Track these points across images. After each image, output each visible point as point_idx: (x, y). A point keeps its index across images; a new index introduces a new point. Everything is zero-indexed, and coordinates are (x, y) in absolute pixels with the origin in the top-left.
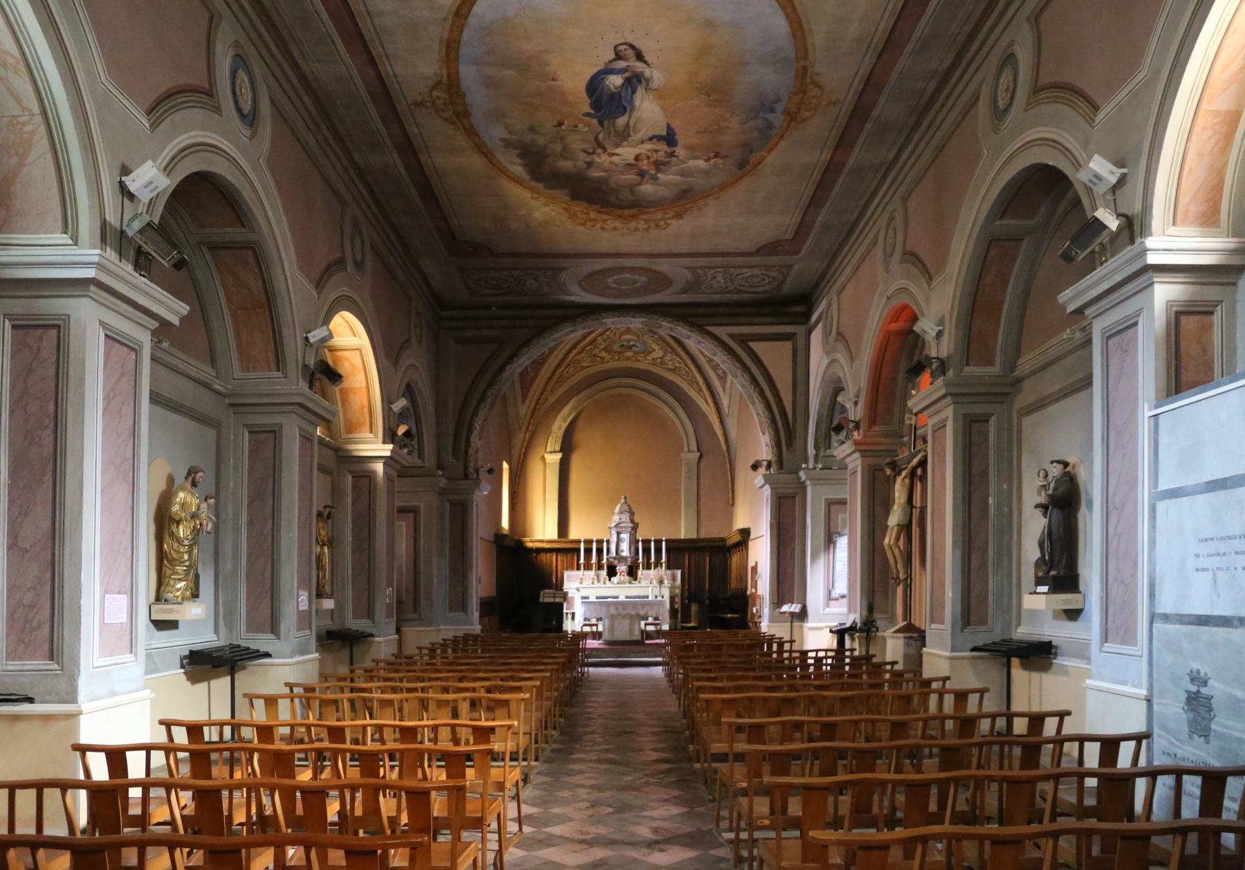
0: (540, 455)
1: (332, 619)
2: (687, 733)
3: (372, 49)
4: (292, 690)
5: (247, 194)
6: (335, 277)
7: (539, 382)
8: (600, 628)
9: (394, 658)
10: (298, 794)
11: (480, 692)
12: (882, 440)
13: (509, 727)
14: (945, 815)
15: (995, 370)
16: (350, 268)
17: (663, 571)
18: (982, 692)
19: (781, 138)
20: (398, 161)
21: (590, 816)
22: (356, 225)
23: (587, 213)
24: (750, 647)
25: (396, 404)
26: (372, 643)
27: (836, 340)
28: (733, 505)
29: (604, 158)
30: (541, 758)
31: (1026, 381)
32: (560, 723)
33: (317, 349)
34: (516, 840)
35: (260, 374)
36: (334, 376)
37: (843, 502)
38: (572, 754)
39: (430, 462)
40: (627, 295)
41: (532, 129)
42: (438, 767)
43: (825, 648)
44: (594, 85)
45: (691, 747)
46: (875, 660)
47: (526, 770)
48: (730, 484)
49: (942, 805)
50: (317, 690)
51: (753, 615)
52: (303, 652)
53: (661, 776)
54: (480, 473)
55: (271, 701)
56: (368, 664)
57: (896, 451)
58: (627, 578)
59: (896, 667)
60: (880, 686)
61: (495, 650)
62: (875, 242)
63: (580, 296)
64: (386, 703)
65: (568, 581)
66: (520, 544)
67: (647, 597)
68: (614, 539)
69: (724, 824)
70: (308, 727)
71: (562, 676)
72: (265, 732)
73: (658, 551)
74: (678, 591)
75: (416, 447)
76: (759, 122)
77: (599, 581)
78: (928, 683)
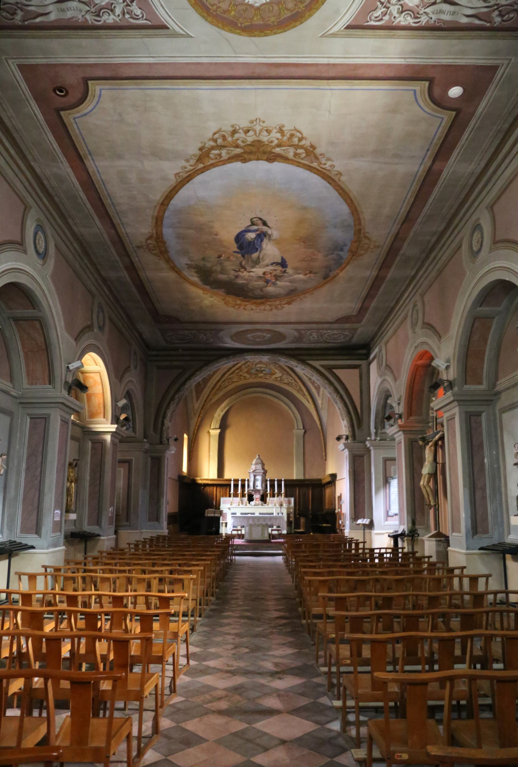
0: (207, 431)
1: (75, 525)
2: (298, 600)
3: (114, 221)
4: (46, 570)
5: (38, 293)
6: (87, 334)
7: (206, 391)
8: (243, 532)
9: (112, 550)
10: (44, 640)
11: (165, 574)
12: (416, 425)
13: (182, 597)
14: (466, 658)
15: (483, 387)
16: (96, 330)
17: (282, 498)
18: (487, 577)
19: (348, 264)
20: (127, 276)
21: (234, 654)
22: (100, 307)
23: (236, 301)
24: (338, 545)
25: (120, 402)
26: (99, 540)
27: (386, 369)
28: (326, 460)
29: (245, 274)
30: (203, 615)
31: (503, 394)
32: (216, 592)
33: (74, 373)
34: (185, 670)
35: (39, 386)
36: (82, 387)
37: (394, 459)
38: (223, 612)
39: (139, 433)
40: (259, 344)
41: (203, 259)
42: (136, 620)
43: (385, 547)
44: (239, 238)
45: (300, 609)
46: (417, 555)
47: (193, 623)
48: (323, 448)
49: (464, 652)
50: (62, 570)
51: (340, 525)
52: (55, 545)
53: (281, 628)
54: (170, 441)
55: (32, 577)
56: (96, 554)
57: (425, 430)
58: (260, 502)
59: (431, 560)
60: (421, 572)
61: (176, 546)
62: (405, 318)
63: (231, 344)
64: (104, 580)
65: (223, 503)
66: (194, 482)
67: (273, 514)
68: (252, 479)
69: (321, 661)
70: (55, 595)
71: (218, 562)
72: (27, 598)
73: (280, 486)
74: (292, 510)
75: (131, 425)
76: (334, 256)
77: (242, 504)
78: (451, 570)
